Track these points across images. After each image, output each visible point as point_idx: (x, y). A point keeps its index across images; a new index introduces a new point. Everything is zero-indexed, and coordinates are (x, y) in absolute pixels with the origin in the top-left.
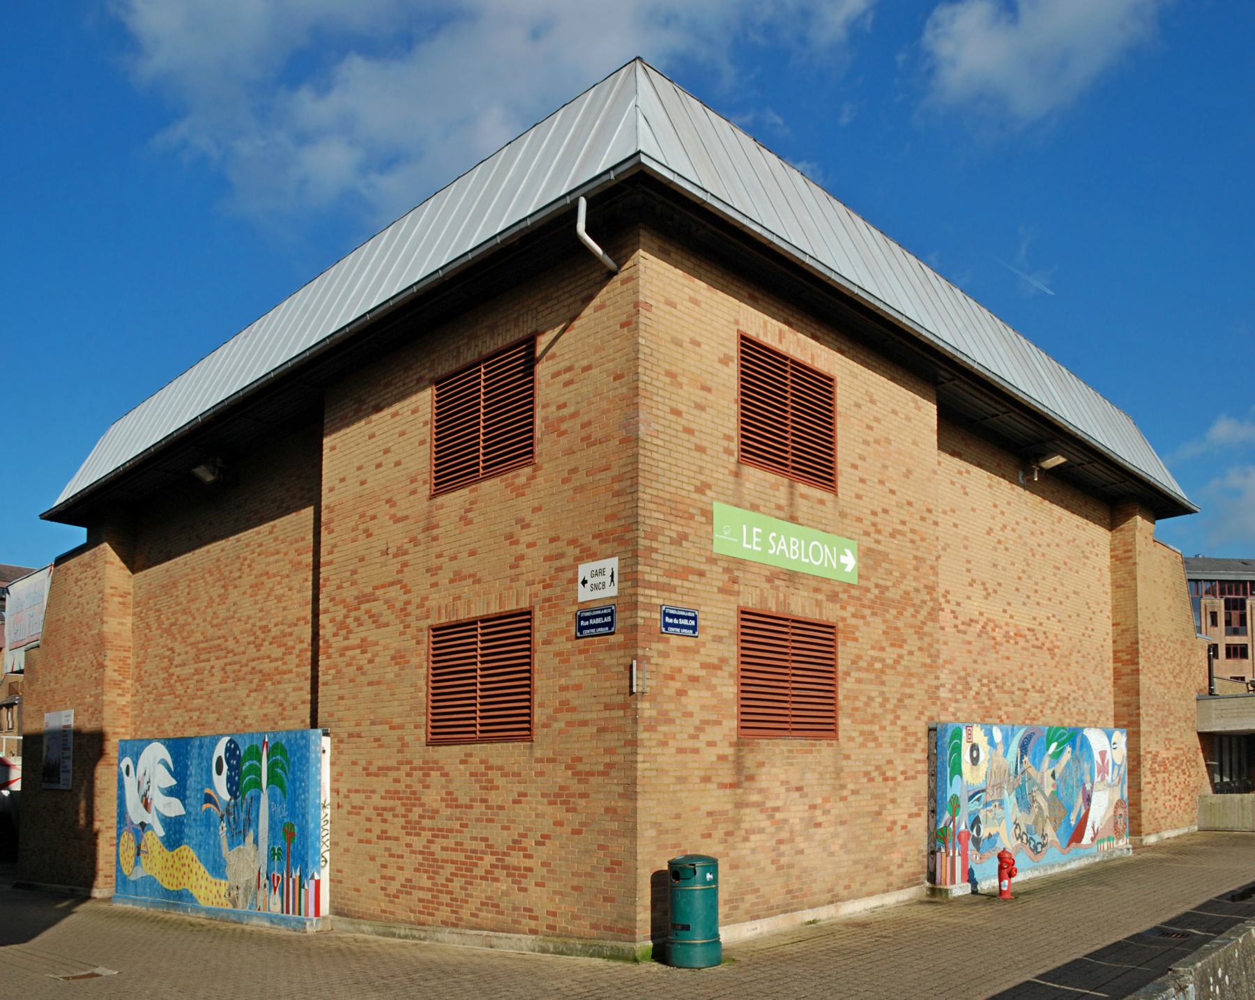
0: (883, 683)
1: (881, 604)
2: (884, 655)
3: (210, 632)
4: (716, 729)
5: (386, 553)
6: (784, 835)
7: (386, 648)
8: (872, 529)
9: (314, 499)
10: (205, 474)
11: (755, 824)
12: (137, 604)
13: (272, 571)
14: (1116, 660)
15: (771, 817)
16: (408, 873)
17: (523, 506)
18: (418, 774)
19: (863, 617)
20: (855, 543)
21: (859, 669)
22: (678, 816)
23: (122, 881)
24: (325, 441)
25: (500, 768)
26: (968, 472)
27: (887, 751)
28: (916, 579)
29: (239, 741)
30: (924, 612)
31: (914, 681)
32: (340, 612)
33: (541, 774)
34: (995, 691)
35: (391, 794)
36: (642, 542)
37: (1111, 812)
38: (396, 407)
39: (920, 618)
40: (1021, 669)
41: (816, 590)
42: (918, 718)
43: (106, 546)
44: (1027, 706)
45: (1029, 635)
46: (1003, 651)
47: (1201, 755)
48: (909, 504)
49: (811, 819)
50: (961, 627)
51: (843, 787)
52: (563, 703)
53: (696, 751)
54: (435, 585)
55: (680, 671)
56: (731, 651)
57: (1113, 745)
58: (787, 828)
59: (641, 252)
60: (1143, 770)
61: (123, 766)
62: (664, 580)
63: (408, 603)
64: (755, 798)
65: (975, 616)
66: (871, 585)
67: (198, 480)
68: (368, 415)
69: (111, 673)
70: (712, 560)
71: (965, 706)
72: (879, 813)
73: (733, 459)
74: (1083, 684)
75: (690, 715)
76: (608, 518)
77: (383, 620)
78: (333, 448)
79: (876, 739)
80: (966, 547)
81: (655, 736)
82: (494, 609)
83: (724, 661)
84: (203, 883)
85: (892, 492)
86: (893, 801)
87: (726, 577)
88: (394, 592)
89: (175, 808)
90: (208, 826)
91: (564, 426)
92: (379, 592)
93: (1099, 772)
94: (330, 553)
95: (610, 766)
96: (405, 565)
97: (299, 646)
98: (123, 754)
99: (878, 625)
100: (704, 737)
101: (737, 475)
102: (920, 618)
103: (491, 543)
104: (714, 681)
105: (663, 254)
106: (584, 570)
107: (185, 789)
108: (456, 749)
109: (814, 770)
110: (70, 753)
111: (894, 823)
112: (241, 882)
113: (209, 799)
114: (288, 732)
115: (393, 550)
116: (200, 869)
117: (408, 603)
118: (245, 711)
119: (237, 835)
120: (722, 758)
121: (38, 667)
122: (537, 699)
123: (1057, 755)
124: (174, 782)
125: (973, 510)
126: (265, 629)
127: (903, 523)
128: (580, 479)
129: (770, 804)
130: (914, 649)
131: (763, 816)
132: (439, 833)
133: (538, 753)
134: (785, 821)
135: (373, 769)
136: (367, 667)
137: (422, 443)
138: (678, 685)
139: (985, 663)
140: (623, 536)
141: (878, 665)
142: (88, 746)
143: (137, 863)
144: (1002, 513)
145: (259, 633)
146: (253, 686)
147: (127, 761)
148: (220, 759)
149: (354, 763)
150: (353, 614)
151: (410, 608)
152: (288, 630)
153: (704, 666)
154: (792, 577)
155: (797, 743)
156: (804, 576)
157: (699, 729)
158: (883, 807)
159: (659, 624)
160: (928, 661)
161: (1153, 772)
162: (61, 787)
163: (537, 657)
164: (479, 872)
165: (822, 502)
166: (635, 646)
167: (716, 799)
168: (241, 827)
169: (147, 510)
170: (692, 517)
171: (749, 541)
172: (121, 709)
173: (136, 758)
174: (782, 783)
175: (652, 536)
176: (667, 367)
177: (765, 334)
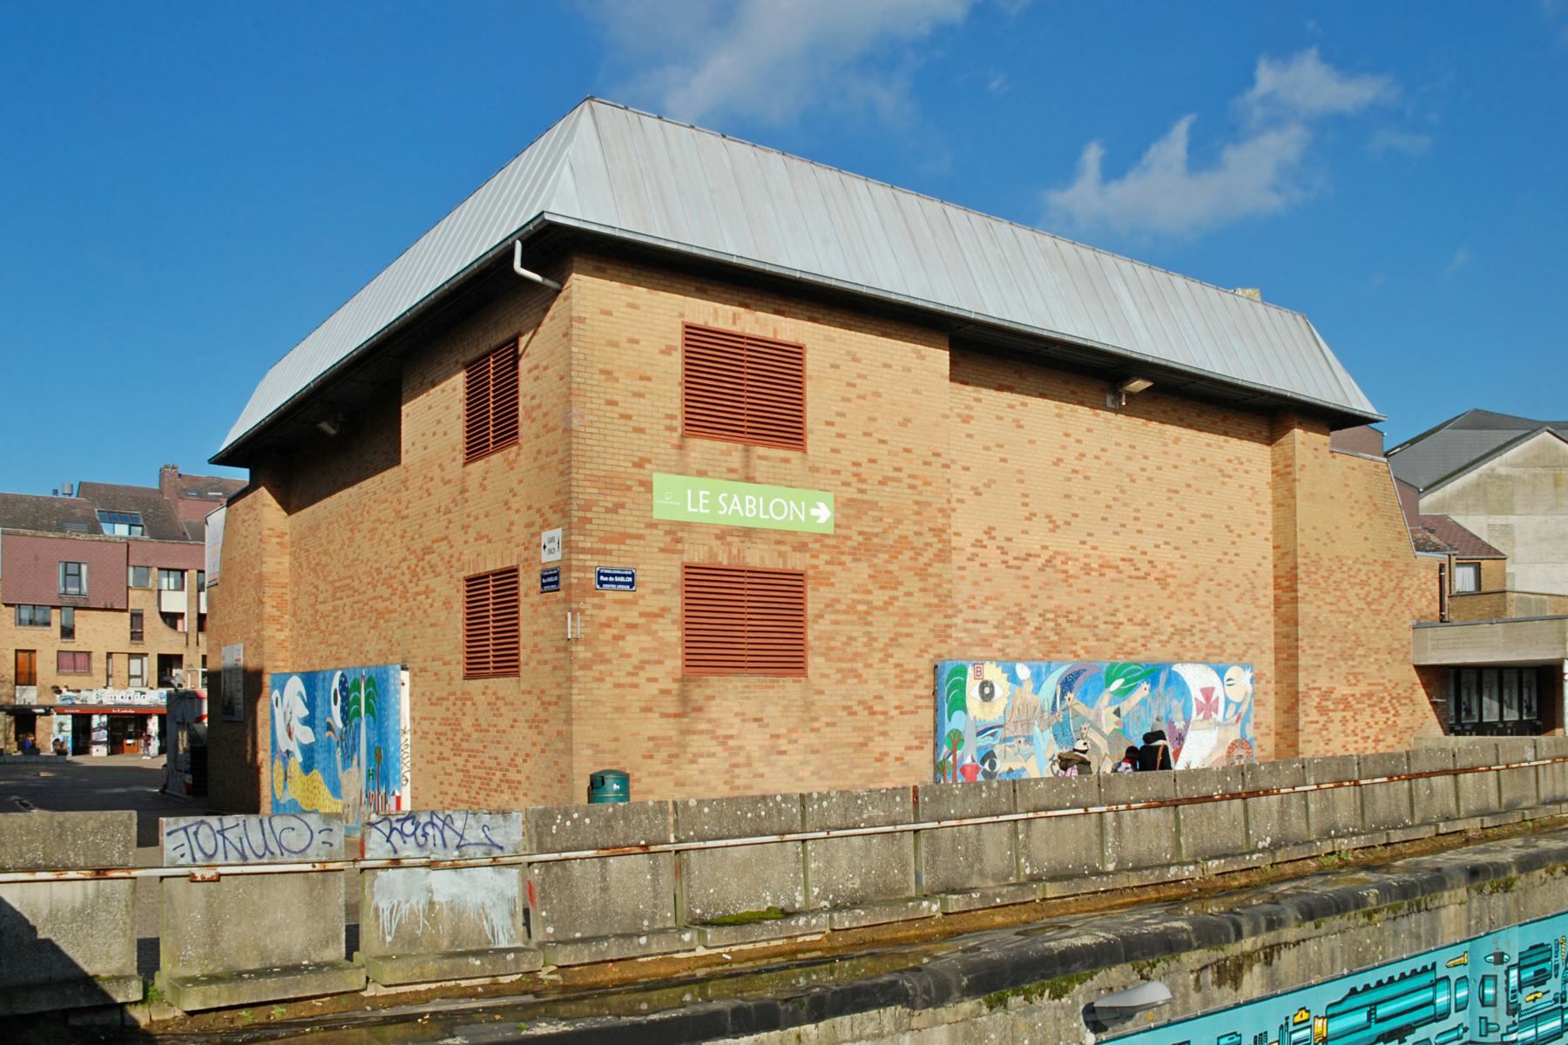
0: (869, 624)
1: (867, 548)
2: (869, 597)
4: (658, 668)
6: (740, 759)
11: (705, 749)
12: (293, 543)
14: (1277, 586)
15: (723, 744)
16: (455, 789)
18: (459, 703)
19: (842, 564)
20: (830, 496)
21: (837, 612)
22: (616, 739)
26: (1024, 404)
28: (915, 523)
31: (911, 620)
33: (524, 703)
36: (575, 513)
37: (1223, 752)
39: (922, 560)
40: (1109, 601)
41: (779, 542)
43: (263, 489)
44: (1120, 640)
46: (1081, 583)
47: (1421, 692)
48: (907, 451)
49: (773, 747)
50: (1011, 563)
51: (815, 719)
52: (536, 645)
53: (636, 686)
55: (617, 619)
56: (675, 602)
58: (742, 753)
59: (574, 275)
60: (1301, 708)
64: (703, 726)
65: (1036, 549)
66: (853, 533)
67: (324, 434)
69: (269, 610)
70: (653, 525)
73: (676, 435)
74: (1217, 614)
75: (629, 656)
79: (859, 676)
81: (590, 673)
82: (499, 566)
85: (883, 442)
86: (884, 734)
87: (668, 539)
88: (444, 546)
90: (329, 751)
95: (559, 697)
100: (643, 675)
101: (680, 447)
102: (922, 560)
104: (654, 627)
105: (599, 272)
106: (546, 536)
109: (776, 704)
111: (886, 754)
116: (325, 791)
118: (367, 647)
122: (522, 641)
123: (1124, 693)
125: (1032, 442)
129: (721, 732)
130: (915, 589)
131: (714, 742)
132: (473, 753)
134: (741, 748)
138: (615, 631)
139: (1050, 597)
140: (563, 509)
142: (253, 681)
147: (276, 693)
153: (642, 615)
154: (748, 533)
156: (763, 531)
157: (641, 666)
158: (871, 739)
159: (595, 582)
161: (1322, 710)
164: (493, 785)
165: (786, 461)
172: (281, 644)
173: (282, 689)
174: (737, 714)
175: (587, 507)
176: (602, 366)
177: (716, 319)
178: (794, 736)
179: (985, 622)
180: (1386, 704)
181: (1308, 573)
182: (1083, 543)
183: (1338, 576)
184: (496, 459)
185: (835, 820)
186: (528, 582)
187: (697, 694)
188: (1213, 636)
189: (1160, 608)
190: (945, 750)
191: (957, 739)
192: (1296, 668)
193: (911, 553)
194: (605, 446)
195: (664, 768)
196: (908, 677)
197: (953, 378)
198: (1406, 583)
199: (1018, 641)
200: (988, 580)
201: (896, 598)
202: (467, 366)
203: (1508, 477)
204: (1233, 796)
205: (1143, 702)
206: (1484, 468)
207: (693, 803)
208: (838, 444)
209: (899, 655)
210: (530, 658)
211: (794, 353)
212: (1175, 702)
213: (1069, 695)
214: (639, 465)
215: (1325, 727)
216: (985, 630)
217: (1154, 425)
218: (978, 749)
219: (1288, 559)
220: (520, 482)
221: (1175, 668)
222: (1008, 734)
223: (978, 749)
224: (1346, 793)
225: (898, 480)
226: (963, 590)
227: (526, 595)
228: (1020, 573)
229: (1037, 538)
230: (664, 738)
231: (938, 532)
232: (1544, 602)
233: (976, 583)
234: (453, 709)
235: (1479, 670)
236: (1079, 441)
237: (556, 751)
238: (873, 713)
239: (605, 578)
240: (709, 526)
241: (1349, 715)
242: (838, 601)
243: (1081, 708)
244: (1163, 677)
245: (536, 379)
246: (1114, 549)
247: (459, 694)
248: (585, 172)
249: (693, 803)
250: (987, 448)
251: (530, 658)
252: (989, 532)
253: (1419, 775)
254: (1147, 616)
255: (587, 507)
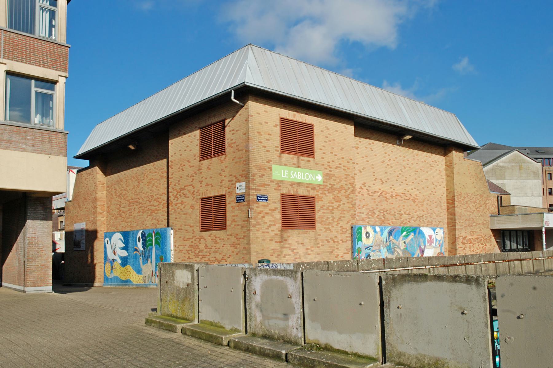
0: (333, 213)
1: (332, 189)
3: (134, 197)
4: (274, 227)
5: (188, 176)
6: (298, 256)
7: (188, 204)
8: (328, 167)
9: (167, 157)
10: (131, 147)
11: (287, 253)
12: (108, 187)
13: (154, 177)
14: (448, 202)
15: (293, 251)
17: (223, 166)
18: (198, 240)
20: (321, 172)
21: (324, 209)
22: (263, 250)
23: (106, 279)
24: (170, 141)
25: (219, 238)
26: (373, 143)
27: (336, 234)
28: (345, 181)
29: (145, 232)
30: (349, 191)
31: (345, 212)
32: (175, 193)
33: (229, 239)
34: (386, 214)
35: (191, 246)
36: (251, 177)
38: (190, 134)
39: (347, 193)
41: (307, 187)
42: (347, 224)
44: (402, 220)
45: (403, 195)
47: (493, 238)
48: (343, 158)
50: (371, 194)
51: (318, 244)
52: (234, 220)
53: (268, 232)
54: (201, 186)
56: (279, 206)
57: (436, 234)
60: (457, 242)
61: (106, 241)
62: (257, 188)
63: (194, 191)
64: (287, 246)
65: (377, 190)
66: (328, 184)
67: (130, 149)
68: (182, 135)
69: (99, 210)
71: (373, 220)
72: (332, 252)
73: (279, 153)
75: (266, 223)
76: (243, 171)
77: (187, 196)
78: (172, 144)
79: (330, 230)
80: (373, 168)
82: (216, 194)
83: (276, 208)
84: (134, 276)
86: (337, 249)
88: (190, 188)
89: (124, 253)
90: (136, 258)
91: (232, 145)
92: (186, 188)
93: (428, 243)
94: (172, 175)
95: (244, 236)
96: (193, 180)
97: (163, 202)
98: (106, 237)
99: (331, 196)
101: (280, 157)
102: (347, 193)
103: (215, 176)
104: (273, 214)
105: (256, 101)
106: (238, 185)
107: (128, 247)
108: (208, 232)
110: (84, 237)
111: (338, 255)
112: (147, 275)
113: (136, 250)
114: (161, 229)
115: (190, 175)
116: (133, 272)
117: (194, 191)
118: (146, 222)
119: (145, 260)
120: (276, 234)
121: (70, 208)
122: (227, 219)
123: (407, 236)
124: (124, 245)
125: (376, 155)
126: (152, 196)
127: (340, 164)
128: (236, 160)
129: (292, 247)
130: (345, 202)
132: (204, 256)
133: (228, 233)
134: (297, 253)
135: (185, 239)
136: (183, 209)
137: (197, 145)
138: (262, 215)
140: (246, 176)
141: (331, 208)
142: (91, 235)
143: (111, 272)
144: (389, 155)
145: (150, 197)
146: (149, 214)
148: (139, 238)
149: (180, 237)
150: (179, 194)
151: (195, 193)
152: (159, 197)
153: (270, 210)
154: (299, 184)
155: (301, 231)
157: (269, 227)
158: (334, 250)
159: (256, 199)
160: (351, 206)
161: (463, 243)
162: (81, 249)
163: (227, 208)
165: (309, 161)
166: (249, 205)
167: (275, 245)
168: (146, 258)
169: (111, 157)
170: (266, 170)
171: (284, 175)
175: (254, 175)
178: (313, 249)
179: (363, 213)
180: (482, 242)
181: (458, 198)
182: (391, 188)
183: (467, 199)
184: (215, 160)
185: (365, 268)
186: (230, 201)
187: (285, 235)
188: (429, 219)
189: (261, 142)
190: (356, 254)
191: (360, 250)
192: (455, 229)
193: (344, 191)
194: (258, 156)
195: (276, 259)
196: (344, 230)
197: (356, 136)
198: (487, 202)
199: (373, 220)
200: (364, 200)
201: (340, 205)
202: (200, 128)
203: (503, 167)
204: (462, 264)
205: (412, 239)
206: (495, 163)
207: (332, 262)
208: (324, 156)
209: (341, 223)
210: (231, 224)
211: (310, 127)
212: (421, 240)
213: (391, 237)
214: (268, 162)
215: (464, 249)
216: (363, 216)
217: (411, 150)
218: (366, 254)
219: (451, 194)
220: (226, 167)
221: (421, 228)
222: (374, 249)
223: (366, 254)
224: (491, 265)
225: (340, 168)
226: (358, 202)
227: (229, 204)
228: (373, 197)
229: (377, 186)
230: (276, 249)
231: (352, 184)
232: (526, 209)
233: (360, 201)
234: (195, 242)
235: (510, 231)
236: (389, 155)
237: (243, 254)
238: (334, 242)
239: (260, 198)
240: (288, 182)
241: (471, 245)
242: (324, 206)
243: (394, 241)
244: (417, 231)
245: (233, 134)
246: (399, 190)
247: (198, 236)
248: (254, 68)
249: (332, 262)
250: (363, 157)
251: (231, 224)
252: (364, 184)
253: (511, 260)
254: (410, 212)
255: (254, 175)
